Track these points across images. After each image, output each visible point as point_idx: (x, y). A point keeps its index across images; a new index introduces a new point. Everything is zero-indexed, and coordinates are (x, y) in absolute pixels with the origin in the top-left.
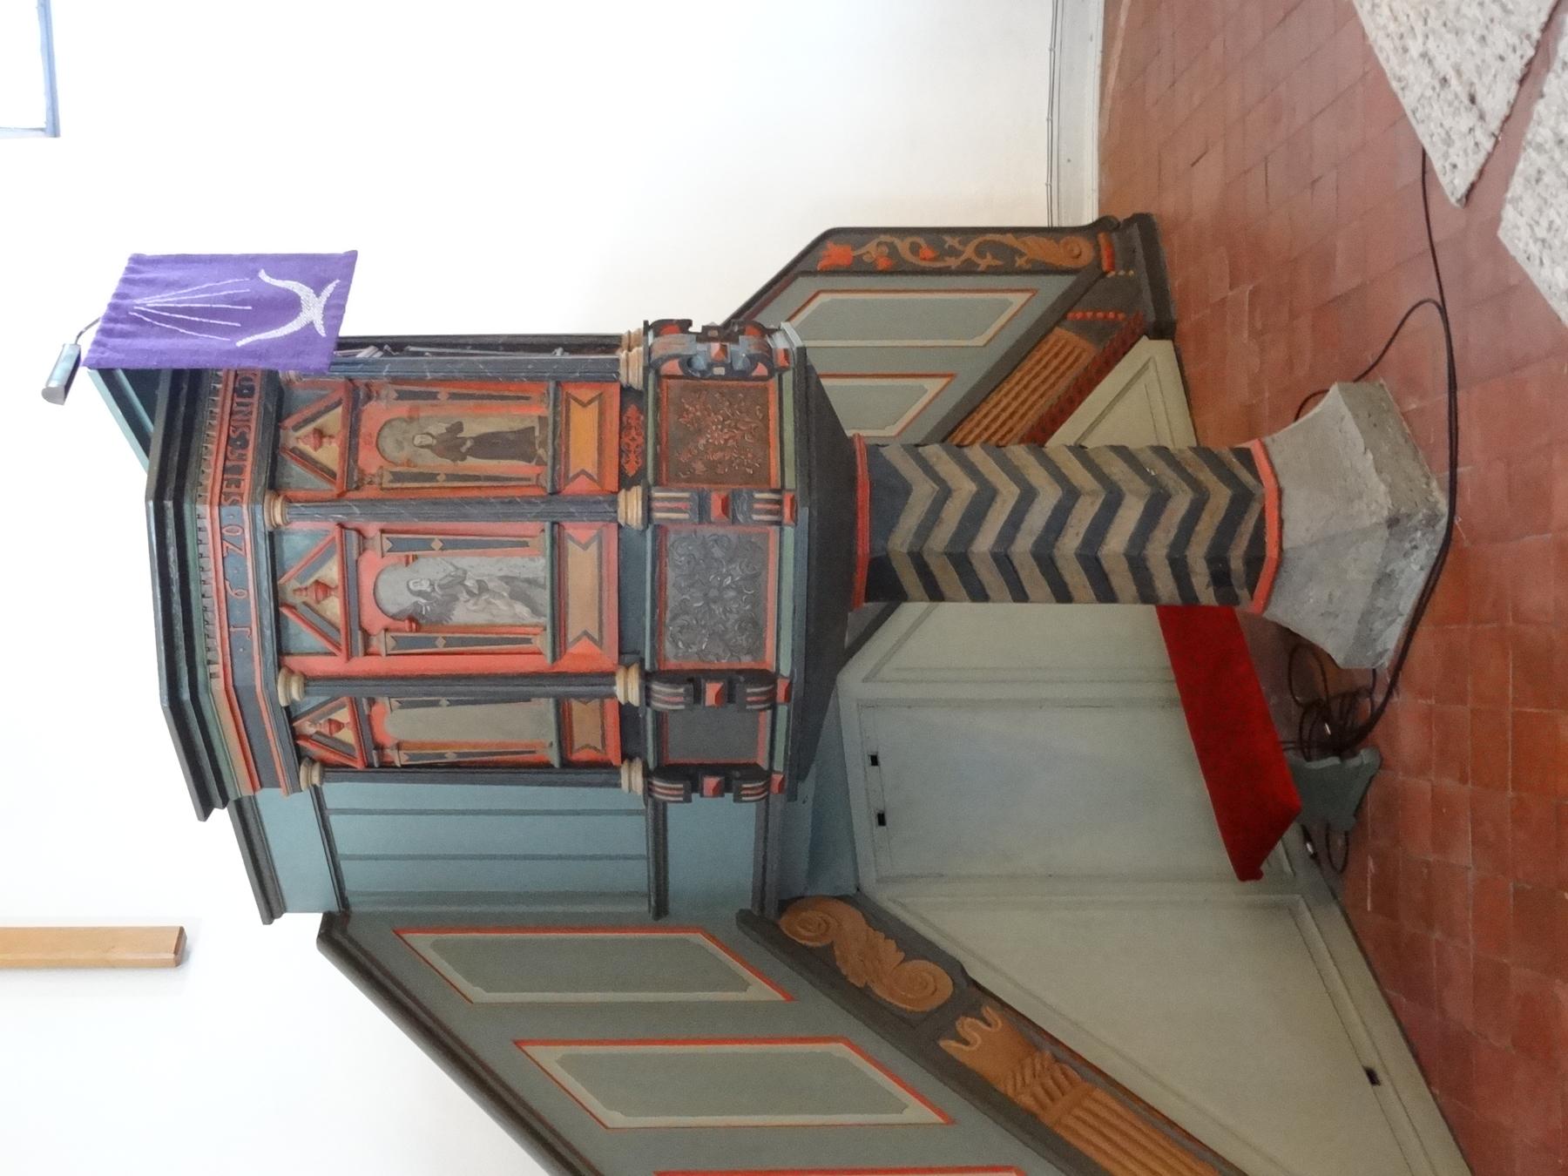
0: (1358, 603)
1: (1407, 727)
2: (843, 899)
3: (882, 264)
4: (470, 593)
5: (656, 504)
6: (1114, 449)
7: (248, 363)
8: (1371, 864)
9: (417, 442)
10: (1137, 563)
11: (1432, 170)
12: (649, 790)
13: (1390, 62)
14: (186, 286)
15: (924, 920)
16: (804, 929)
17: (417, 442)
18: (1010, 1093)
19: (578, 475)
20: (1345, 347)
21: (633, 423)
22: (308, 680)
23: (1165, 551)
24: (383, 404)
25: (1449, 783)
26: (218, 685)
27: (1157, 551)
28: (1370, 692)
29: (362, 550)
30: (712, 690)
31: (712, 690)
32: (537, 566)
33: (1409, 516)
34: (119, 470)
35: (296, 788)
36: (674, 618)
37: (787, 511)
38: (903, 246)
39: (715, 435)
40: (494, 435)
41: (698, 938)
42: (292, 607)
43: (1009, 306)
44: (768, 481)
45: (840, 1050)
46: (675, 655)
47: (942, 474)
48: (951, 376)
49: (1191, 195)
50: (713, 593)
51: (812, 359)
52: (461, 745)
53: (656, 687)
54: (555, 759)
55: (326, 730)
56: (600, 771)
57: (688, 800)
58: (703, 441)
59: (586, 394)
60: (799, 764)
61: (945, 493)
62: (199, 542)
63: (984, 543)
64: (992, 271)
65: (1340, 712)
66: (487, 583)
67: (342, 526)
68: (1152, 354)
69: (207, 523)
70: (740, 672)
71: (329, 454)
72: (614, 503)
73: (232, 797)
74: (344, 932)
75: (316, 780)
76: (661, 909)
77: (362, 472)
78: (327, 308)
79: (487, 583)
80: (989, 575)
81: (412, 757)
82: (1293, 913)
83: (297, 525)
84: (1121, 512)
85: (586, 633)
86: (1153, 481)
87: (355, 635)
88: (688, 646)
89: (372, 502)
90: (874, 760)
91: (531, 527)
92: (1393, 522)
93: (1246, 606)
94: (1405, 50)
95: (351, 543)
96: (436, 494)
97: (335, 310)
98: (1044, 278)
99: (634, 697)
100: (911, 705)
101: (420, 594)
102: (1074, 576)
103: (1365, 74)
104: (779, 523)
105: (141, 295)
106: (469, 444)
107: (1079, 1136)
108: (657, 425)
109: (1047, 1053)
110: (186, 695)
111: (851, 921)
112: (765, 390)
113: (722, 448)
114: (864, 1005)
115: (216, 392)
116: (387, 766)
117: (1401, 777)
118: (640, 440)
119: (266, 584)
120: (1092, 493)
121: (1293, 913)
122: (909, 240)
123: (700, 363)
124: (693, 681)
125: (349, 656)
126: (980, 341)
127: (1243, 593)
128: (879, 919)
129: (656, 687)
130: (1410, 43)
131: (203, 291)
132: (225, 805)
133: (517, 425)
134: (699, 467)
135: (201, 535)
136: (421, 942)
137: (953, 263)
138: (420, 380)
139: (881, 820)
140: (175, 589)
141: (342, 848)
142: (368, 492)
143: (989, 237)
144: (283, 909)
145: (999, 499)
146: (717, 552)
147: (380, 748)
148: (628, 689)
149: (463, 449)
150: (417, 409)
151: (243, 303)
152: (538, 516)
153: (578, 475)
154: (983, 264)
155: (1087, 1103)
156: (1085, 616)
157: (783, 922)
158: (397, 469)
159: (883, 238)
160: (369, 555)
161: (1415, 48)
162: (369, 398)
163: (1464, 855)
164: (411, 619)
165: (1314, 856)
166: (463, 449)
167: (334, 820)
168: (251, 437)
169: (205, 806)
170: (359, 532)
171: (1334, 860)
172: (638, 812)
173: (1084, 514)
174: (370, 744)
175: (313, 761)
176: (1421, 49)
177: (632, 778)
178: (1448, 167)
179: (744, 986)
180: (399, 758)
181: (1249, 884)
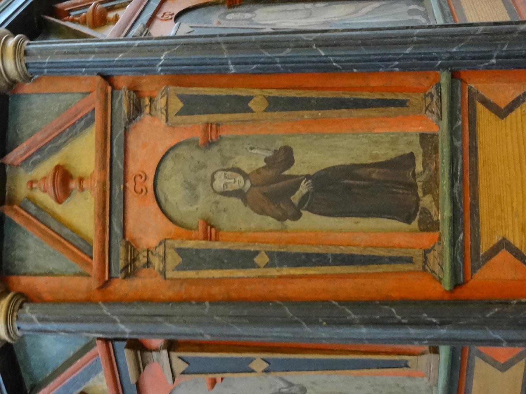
9: (219, 184)
15: (273, 12)
17: (219, 184)
29: (140, 367)
40: (348, 171)
77: (131, 248)
106: (304, 188)
133: (385, 153)
142: (145, 283)
149: (296, 198)
153: (495, 250)
166: (296, 198)
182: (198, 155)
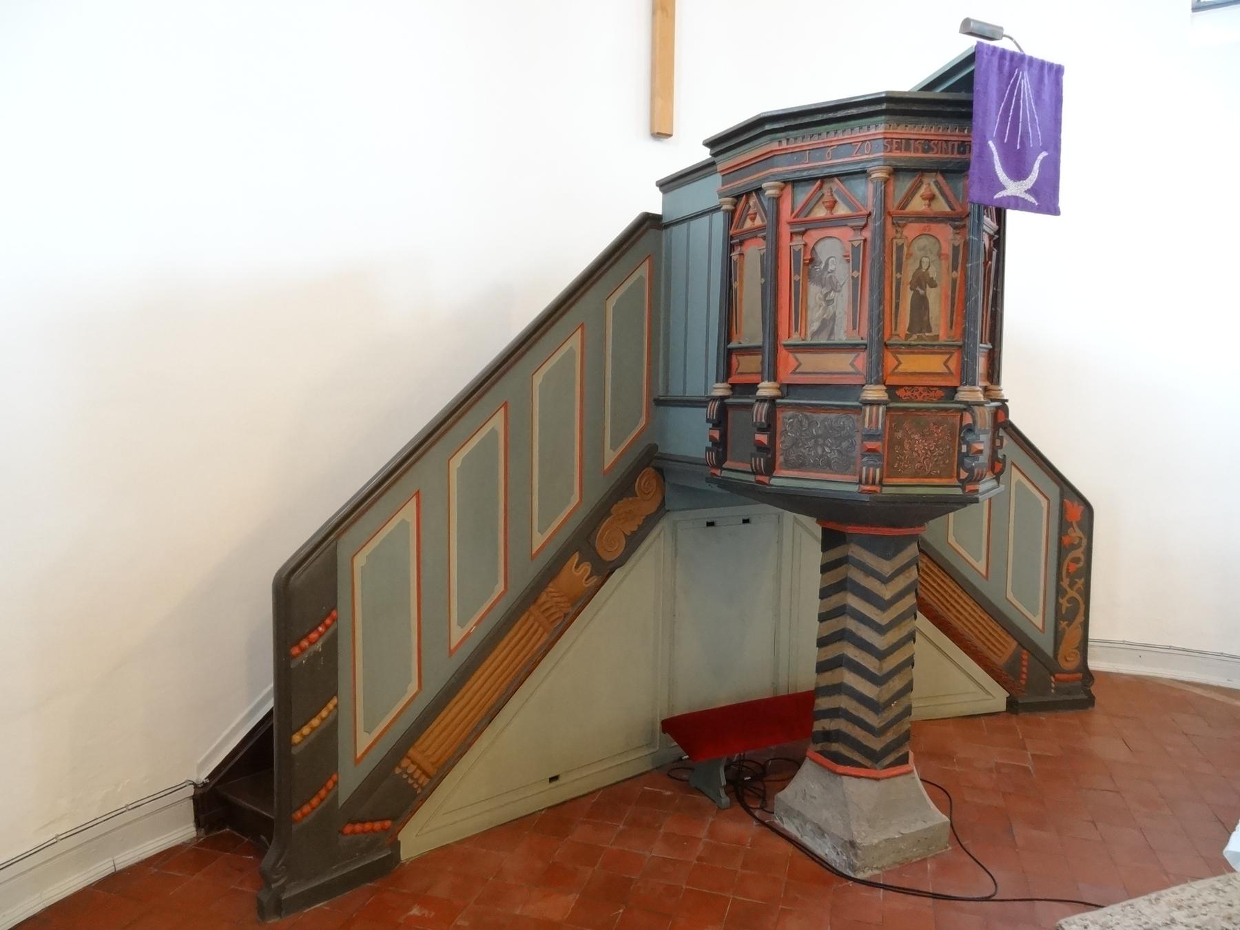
0: (809, 814)
1: (739, 829)
2: (663, 503)
3: (1066, 540)
4: (826, 295)
5: (875, 408)
6: (912, 681)
7: (975, 149)
8: (668, 793)
10: (839, 689)
11: (1088, 910)
12: (714, 399)
13: (1170, 895)
14: (1036, 104)
16: (646, 481)
18: (549, 589)
19: (897, 359)
20: (971, 829)
21: (932, 394)
22: (777, 200)
23: (843, 706)
24: (951, 236)
25: (700, 849)
26: (775, 146)
27: (844, 702)
28: (762, 808)
29: (854, 228)
30: (763, 438)
31: (763, 438)
32: (841, 336)
33: (856, 855)
34: (908, 77)
35: (721, 195)
36: (807, 418)
37: (868, 488)
38: (1079, 553)
39: (920, 445)
40: (927, 308)
41: (642, 422)
42: (821, 187)
43: (1035, 615)
44: (888, 477)
45: (575, 499)
46: (784, 417)
47: (896, 579)
48: (987, 577)
49: (1105, 739)
50: (820, 441)
51: (972, 507)
52: (741, 291)
53: (766, 405)
54: (733, 345)
55: (751, 211)
56: (726, 371)
57: (708, 421)
58: (916, 437)
59: (953, 364)
60: (725, 484)
61: (885, 581)
62: (861, 128)
63: (853, 601)
64: (1058, 607)
65: (754, 787)
66: (833, 304)
67: (870, 214)
68: (997, 698)
69: (873, 131)
70: (774, 455)
71: (918, 205)
72: (877, 383)
73: (716, 159)
74: (651, 227)
75: (724, 207)
76: (659, 402)
77: (905, 225)
78: (1016, 198)
79: (833, 304)
80: (835, 601)
81: (736, 263)
82: (648, 745)
83: (871, 186)
84: (869, 684)
85: (800, 365)
86: (888, 704)
87: (804, 226)
88: (791, 424)
89: (884, 235)
90: (746, 521)
91: (865, 330)
92: (852, 844)
93: (812, 749)
94: (1179, 908)
95: (860, 221)
96: (887, 274)
97: (1019, 204)
98: (1052, 635)
99: (761, 393)
100: (780, 543)
101: (827, 264)
102: (832, 651)
103: (1167, 874)
104: (860, 482)
105: (1030, 75)
107: (522, 625)
108: (928, 409)
109: (570, 610)
110: (767, 127)
111: (650, 507)
112: (951, 477)
113: (912, 449)
114: (601, 513)
115: (962, 130)
116: (732, 248)
117: (711, 819)
118: (920, 398)
119: (834, 170)
120: (880, 669)
121: (648, 745)
122: (1082, 557)
123: (970, 437)
124: (769, 427)
125: (791, 224)
126: (1010, 596)
127: (818, 747)
128: (650, 522)
129: (766, 405)
130: (1184, 912)
131: (1033, 119)
132: (714, 155)
134: (899, 435)
135: (816, 137)
136: (644, 271)
137: (1065, 583)
138: (966, 260)
139: (710, 524)
140: (831, 115)
141: (694, 223)
142: (890, 230)
143: (1082, 607)
144: (664, 192)
145: (879, 612)
146: (844, 444)
147: (741, 243)
148: (767, 389)
150: (947, 258)
151: (1022, 143)
152: (870, 336)
153: (897, 359)
154: (1063, 601)
155: (541, 629)
156: (811, 655)
157: (650, 470)
158: (905, 248)
159: (1085, 542)
160: (851, 232)
161: (1180, 916)
162: (955, 228)
163: (658, 850)
164: (812, 260)
165: (680, 759)
167: (706, 219)
168: (930, 155)
169: (711, 144)
170: (865, 226)
171: (670, 772)
172: (685, 391)
173: (869, 662)
174: (808, 226)
175: (735, 205)
176: (1178, 920)
177: (720, 389)
178: (1086, 923)
179: (614, 448)
180: (735, 256)
181: (659, 725)
182: (935, 251)
